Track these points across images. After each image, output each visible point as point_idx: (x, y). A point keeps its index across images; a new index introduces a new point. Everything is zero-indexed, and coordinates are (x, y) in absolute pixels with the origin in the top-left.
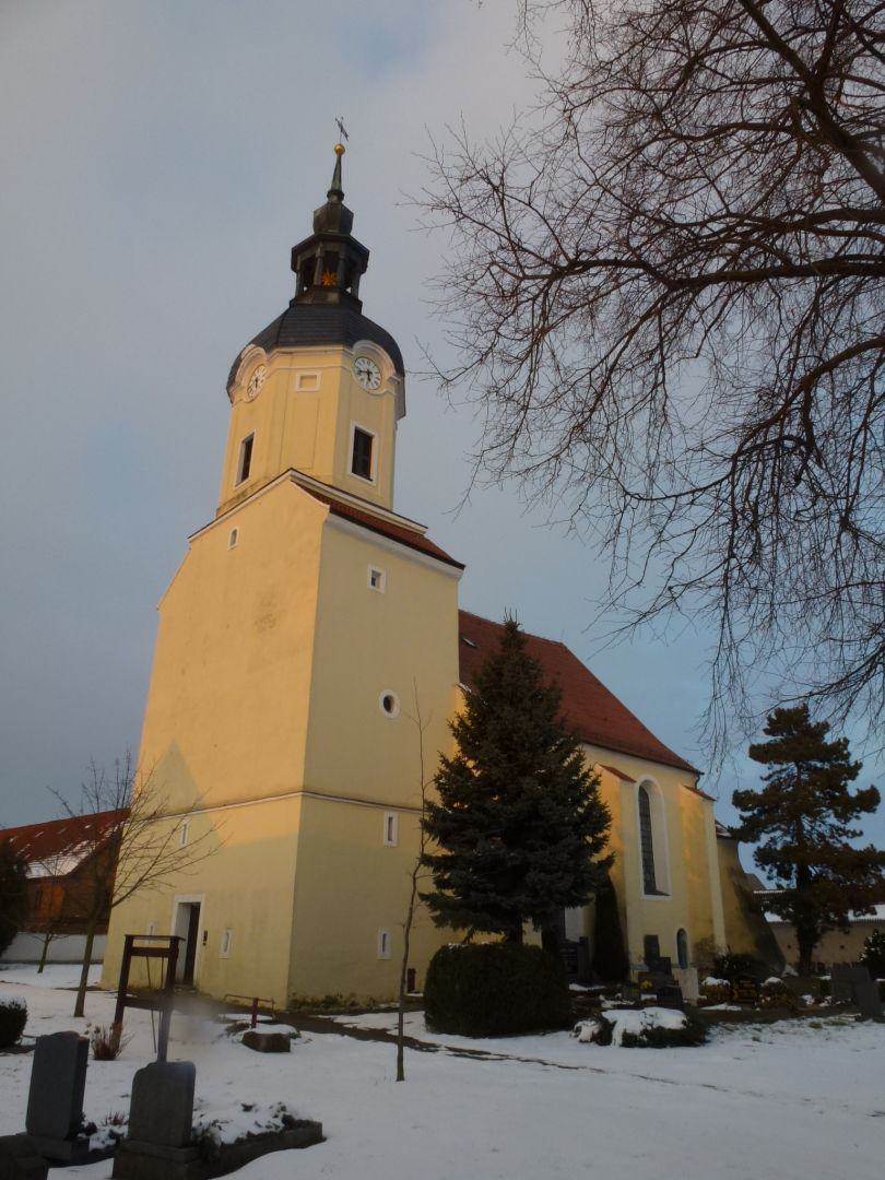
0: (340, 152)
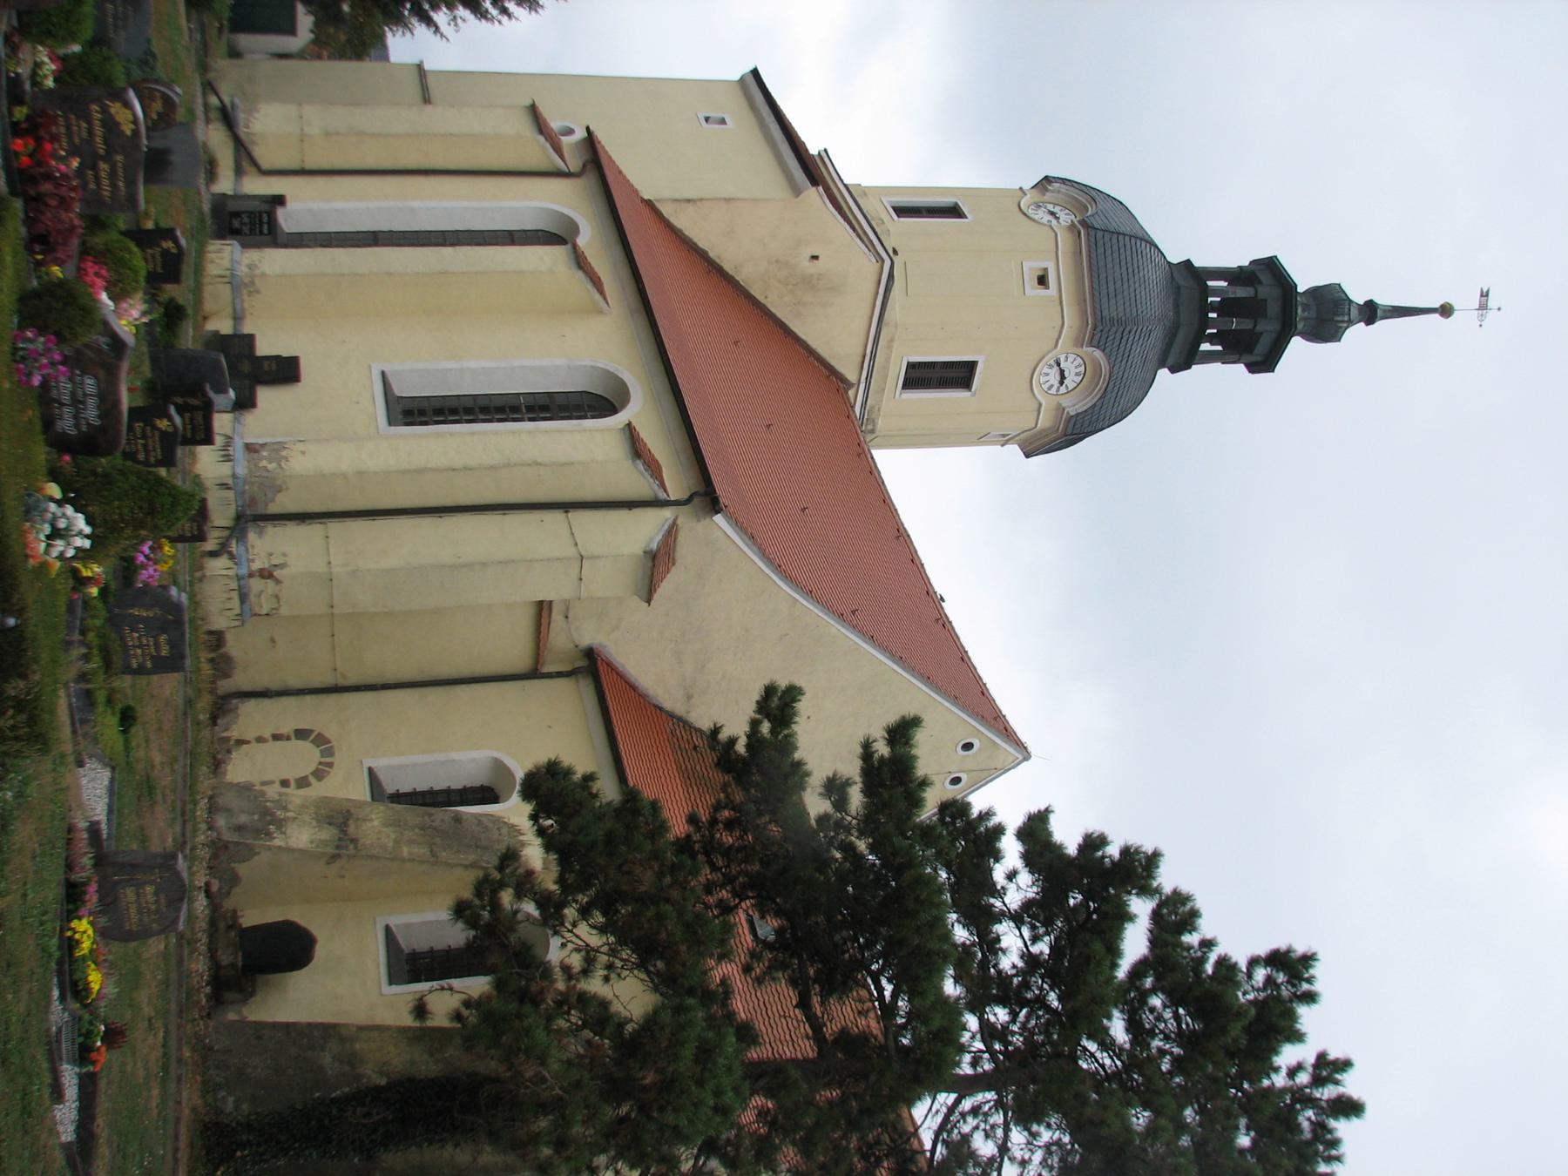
0: (1446, 311)
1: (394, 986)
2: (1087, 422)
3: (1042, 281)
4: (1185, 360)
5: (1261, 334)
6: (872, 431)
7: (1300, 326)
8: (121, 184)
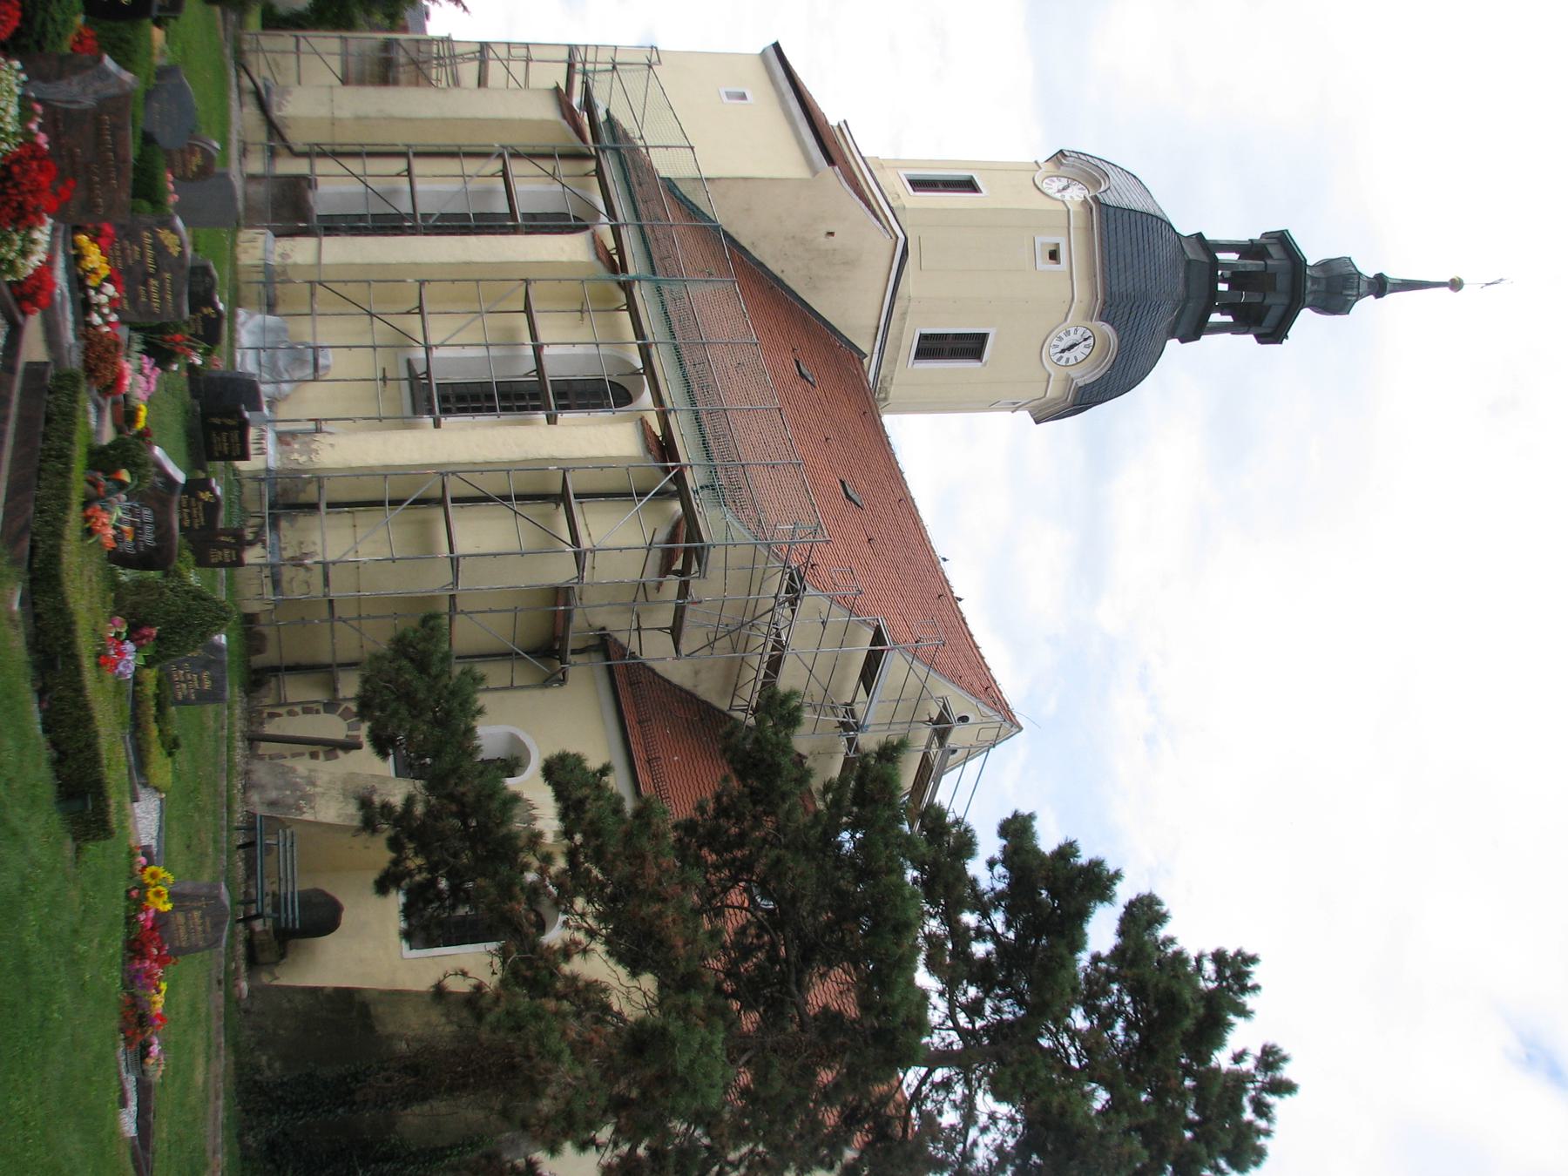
0: (1455, 285)
1: (414, 951)
2: (1095, 393)
3: (1054, 255)
4: (1193, 330)
5: (1269, 307)
6: (885, 399)
7: (1309, 299)
8: (169, 297)
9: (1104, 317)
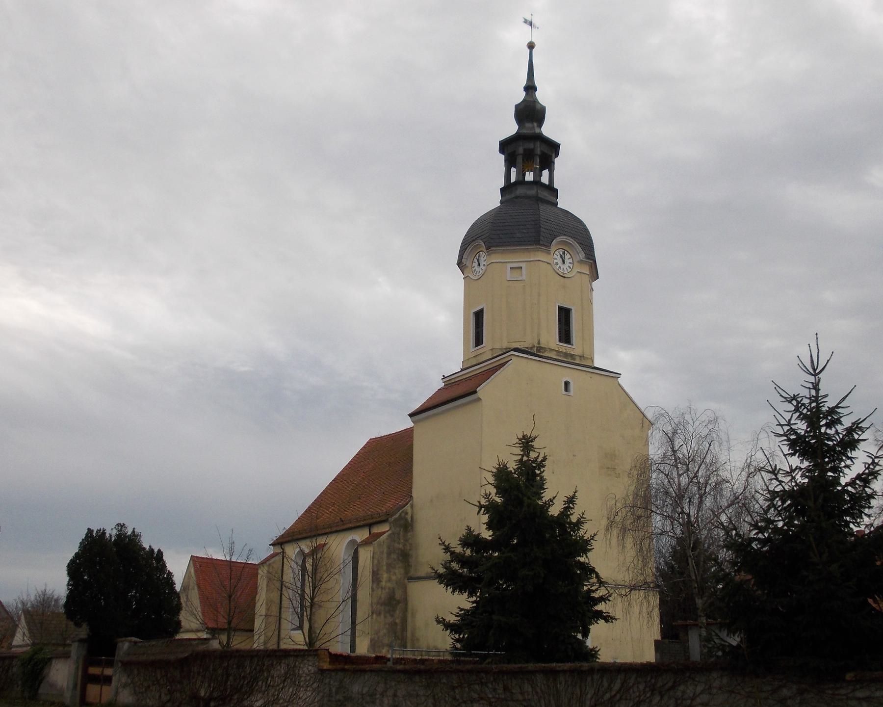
9: (549, 246)
